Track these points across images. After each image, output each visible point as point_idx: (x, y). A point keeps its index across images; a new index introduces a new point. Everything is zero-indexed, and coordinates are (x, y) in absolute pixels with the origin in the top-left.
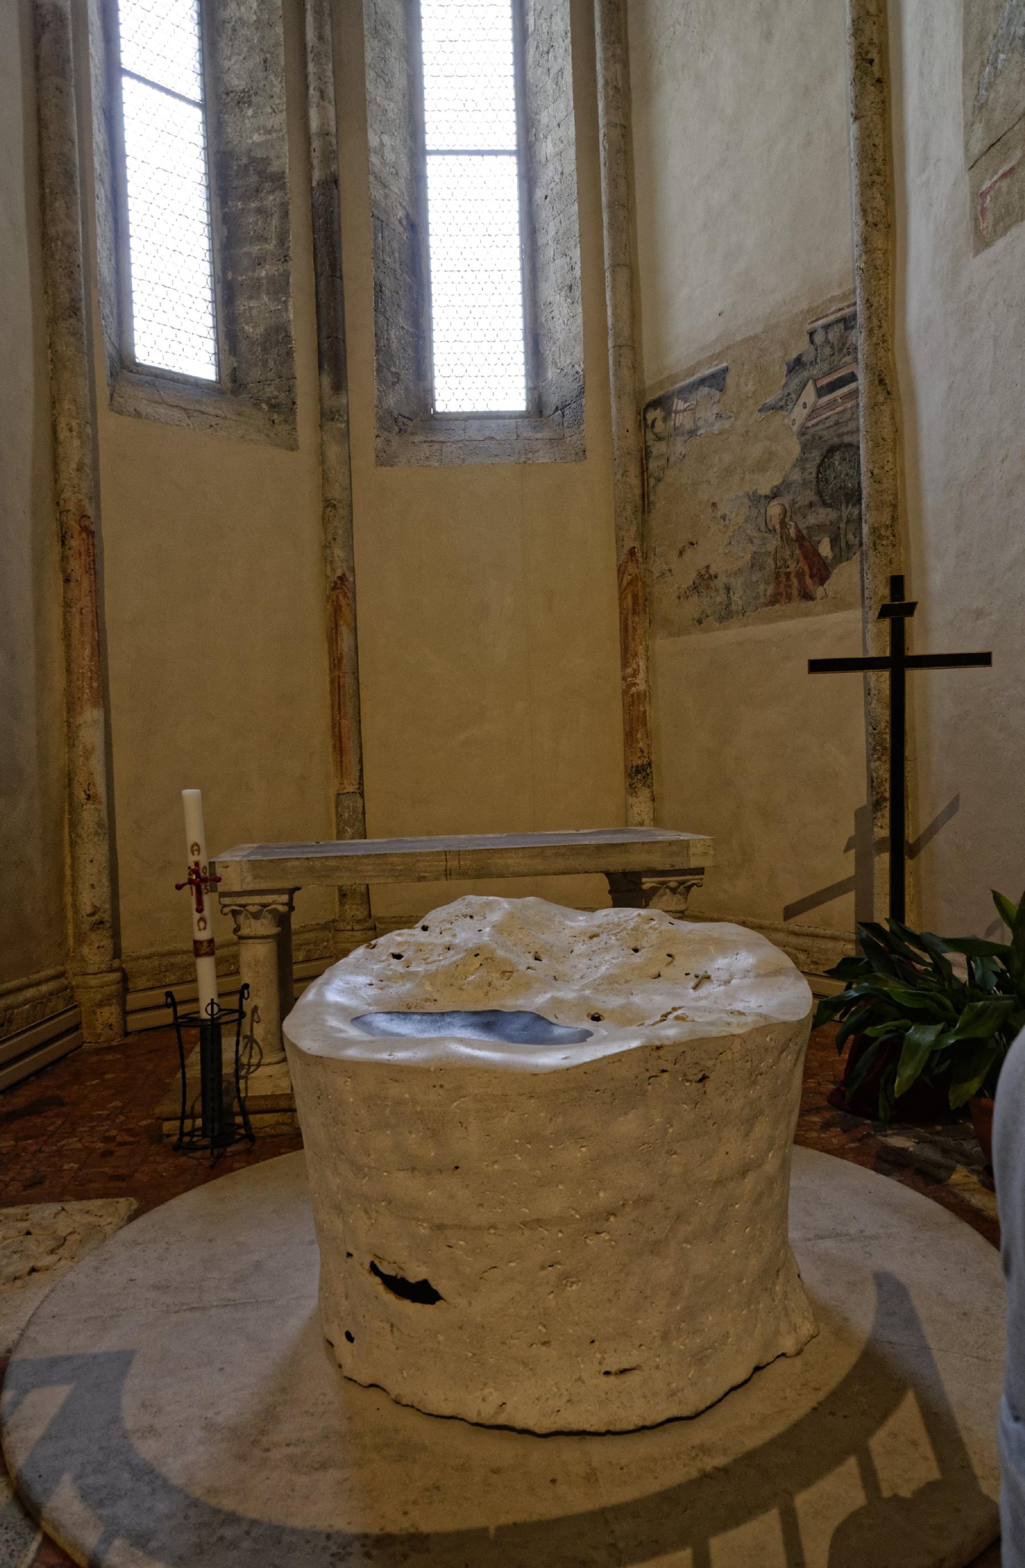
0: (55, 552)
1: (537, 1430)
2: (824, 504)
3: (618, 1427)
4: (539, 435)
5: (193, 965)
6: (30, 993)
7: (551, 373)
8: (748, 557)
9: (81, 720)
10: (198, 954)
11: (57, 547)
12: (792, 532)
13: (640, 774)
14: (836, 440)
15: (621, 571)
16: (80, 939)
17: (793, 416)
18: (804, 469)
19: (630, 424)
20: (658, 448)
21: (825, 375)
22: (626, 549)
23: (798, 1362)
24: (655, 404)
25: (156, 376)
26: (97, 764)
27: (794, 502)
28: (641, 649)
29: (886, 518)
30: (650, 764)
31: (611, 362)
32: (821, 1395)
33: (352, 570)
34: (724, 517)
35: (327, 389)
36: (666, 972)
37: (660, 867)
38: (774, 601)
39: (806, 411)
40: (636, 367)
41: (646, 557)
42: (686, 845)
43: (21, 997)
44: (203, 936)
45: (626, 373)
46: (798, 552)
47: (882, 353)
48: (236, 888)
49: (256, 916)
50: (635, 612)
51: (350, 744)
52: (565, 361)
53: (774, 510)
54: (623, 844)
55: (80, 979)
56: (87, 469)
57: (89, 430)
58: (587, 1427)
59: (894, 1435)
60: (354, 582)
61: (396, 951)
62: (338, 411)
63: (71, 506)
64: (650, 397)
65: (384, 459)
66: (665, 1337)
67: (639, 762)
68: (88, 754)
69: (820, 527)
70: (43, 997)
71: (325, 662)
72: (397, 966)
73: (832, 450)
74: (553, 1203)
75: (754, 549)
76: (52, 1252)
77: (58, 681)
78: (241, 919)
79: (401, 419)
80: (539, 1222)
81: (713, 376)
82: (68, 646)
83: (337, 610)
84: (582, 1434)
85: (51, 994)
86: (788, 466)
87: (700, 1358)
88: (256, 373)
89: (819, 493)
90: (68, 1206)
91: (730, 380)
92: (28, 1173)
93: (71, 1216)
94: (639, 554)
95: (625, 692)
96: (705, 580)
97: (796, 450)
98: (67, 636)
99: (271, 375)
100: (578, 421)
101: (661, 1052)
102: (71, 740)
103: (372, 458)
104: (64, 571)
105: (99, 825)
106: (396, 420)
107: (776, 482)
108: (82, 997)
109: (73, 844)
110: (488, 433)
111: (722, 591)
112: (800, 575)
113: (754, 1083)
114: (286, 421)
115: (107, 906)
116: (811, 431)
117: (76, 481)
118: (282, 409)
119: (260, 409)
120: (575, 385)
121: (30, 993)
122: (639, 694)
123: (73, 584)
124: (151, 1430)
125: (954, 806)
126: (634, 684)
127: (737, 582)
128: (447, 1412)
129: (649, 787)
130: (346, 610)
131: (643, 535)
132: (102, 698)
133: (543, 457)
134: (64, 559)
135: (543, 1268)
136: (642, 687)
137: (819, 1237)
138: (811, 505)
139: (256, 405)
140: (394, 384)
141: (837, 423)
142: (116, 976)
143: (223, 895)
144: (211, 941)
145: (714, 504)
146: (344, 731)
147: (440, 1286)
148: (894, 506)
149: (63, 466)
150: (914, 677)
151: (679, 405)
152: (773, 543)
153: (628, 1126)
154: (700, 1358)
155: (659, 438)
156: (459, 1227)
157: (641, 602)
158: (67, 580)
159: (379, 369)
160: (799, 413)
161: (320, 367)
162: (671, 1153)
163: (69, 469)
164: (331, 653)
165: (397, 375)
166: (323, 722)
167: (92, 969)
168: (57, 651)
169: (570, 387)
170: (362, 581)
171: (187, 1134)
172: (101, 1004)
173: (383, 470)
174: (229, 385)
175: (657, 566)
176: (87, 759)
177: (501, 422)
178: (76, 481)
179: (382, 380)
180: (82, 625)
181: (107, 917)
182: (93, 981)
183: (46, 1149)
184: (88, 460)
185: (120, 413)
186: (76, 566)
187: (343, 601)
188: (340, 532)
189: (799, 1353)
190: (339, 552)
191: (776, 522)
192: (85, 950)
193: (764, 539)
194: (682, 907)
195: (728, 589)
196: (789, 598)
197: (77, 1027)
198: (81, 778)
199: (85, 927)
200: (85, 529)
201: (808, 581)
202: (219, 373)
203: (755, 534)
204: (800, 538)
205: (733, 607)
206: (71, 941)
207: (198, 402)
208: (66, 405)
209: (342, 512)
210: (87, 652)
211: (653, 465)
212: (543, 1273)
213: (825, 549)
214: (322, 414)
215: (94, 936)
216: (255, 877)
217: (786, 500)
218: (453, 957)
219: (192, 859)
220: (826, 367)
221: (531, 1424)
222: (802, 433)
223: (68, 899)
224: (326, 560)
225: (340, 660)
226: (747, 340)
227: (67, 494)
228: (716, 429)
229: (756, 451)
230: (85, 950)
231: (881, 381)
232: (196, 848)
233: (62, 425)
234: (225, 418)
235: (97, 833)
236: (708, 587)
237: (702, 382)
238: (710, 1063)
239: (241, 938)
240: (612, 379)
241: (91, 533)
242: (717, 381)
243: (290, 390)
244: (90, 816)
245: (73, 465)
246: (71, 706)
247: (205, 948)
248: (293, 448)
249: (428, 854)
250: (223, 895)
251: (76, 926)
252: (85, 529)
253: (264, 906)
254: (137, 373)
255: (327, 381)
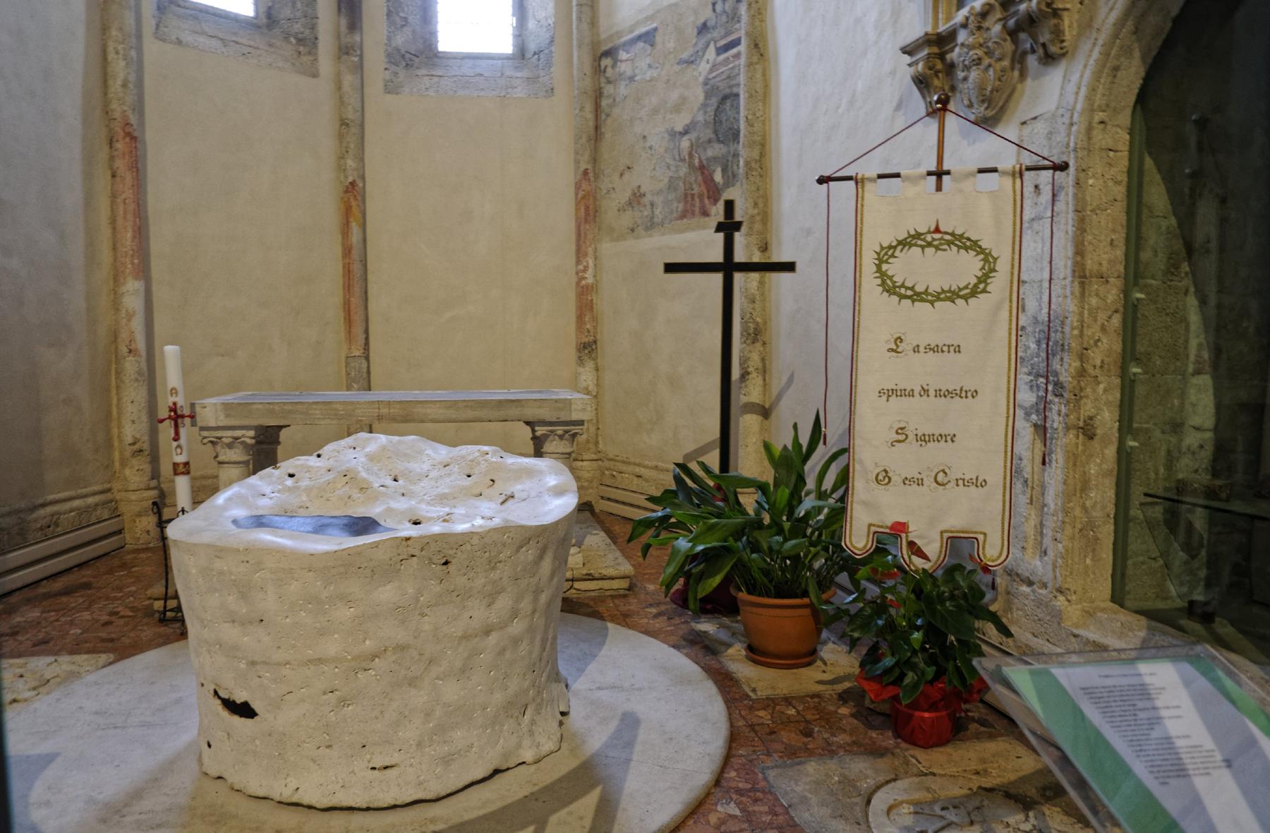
0: (103, 154)
1: (318, 806)
2: (719, 141)
3: (376, 805)
4: (519, 75)
5: (173, 481)
6: (76, 503)
7: (531, 24)
8: (666, 180)
9: (124, 289)
10: (176, 474)
11: (106, 149)
12: (696, 162)
13: (588, 348)
14: (728, 91)
15: (578, 186)
16: (124, 463)
17: (700, 69)
18: (706, 112)
19: (588, 69)
20: (608, 90)
21: (722, 38)
22: (582, 169)
23: (533, 767)
24: (607, 54)
25: (201, 11)
26: (137, 325)
27: (698, 138)
28: (590, 250)
29: (755, 154)
30: (595, 342)
31: (574, 17)
32: (536, 788)
33: (363, 178)
34: (651, 148)
35: (344, 28)
36: (486, 492)
37: (548, 419)
38: (683, 216)
39: (708, 66)
40: (593, 23)
41: (597, 177)
42: (568, 403)
43: (68, 506)
44: (180, 459)
45: (585, 26)
46: (700, 178)
47: (757, 23)
48: (212, 424)
49: (230, 446)
50: (586, 221)
51: (358, 318)
52: (541, 14)
53: (685, 143)
54: (519, 401)
55: (123, 494)
56: (131, 86)
57: (133, 53)
58: (354, 805)
59: (570, 813)
60: (364, 187)
61: (291, 472)
62: (352, 47)
63: (117, 115)
64: (604, 48)
65: (391, 88)
66: (419, 745)
67: (586, 340)
68: (130, 317)
69: (715, 159)
70: (89, 507)
71: (339, 250)
72: (290, 482)
73: (725, 98)
74: (332, 647)
75: (671, 174)
76: (34, 689)
77: (106, 256)
78: (218, 448)
79: (408, 56)
80: (320, 661)
81: (647, 34)
82: (114, 229)
83: (347, 211)
84: (351, 809)
85: (97, 505)
86: (695, 109)
87: (446, 761)
88: (287, 12)
89: (716, 132)
90: (60, 659)
91: (659, 39)
92: (41, 636)
93: (65, 663)
94: (591, 175)
95: (578, 284)
96: (637, 197)
97: (701, 97)
98: (113, 221)
99: (298, 14)
100: (549, 64)
101: (409, 542)
102: (116, 305)
103: (380, 85)
104: (111, 169)
105: (139, 373)
106: (403, 56)
107: (687, 122)
108: (123, 508)
109: (118, 387)
110: (478, 71)
111: (649, 207)
112: (701, 196)
113: (494, 568)
114: (310, 53)
115: (146, 438)
116: (711, 82)
117: (121, 95)
118: (307, 43)
119: (290, 42)
120: (548, 35)
121: (76, 503)
122: (587, 286)
123: (118, 179)
124: (48, 804)
125: (790, 380)
126: (584, 278)
127: (659, 200)
128: (261, 794)
129: (595, 359)
130: (355, 210)
131: (594, 160)
132: (144, 271)
133: (520, 93)
134: (112, 158)
135: (325, 693)
136: (590, 280)
137: (599, 688)
138: (710, 141)
139: (286, 39)
140: (403, 26)
141: (729, 77)
142: (154, 493)
143: (202, 429)
144: (186, 464)
145: (645, 137)
146: (352, 307)
147: (255, 706)
148: (763, 145)
149: (110, 82)
150: (717, 279)
151: (623, 55)
152: (684, 170)
153: (386, 594)
154: (446, 761)
155: (609, 82)
156: (265, 663)
157: (592, 213)
158: (114, 176)
159: (389, 14)
160: (704, 67)
161: (339, 9)
162: (423, 615)
163: (116, 86)
164: (343, 245)
165: (405, 19)
166: (338, 299)
167: (132, 487)
168: (106, 232)
169: (545, 36)
170: (372, 189)
171: (171, 610)
172: (139, 515)
173: (389, 97)
174: (265, 21)
175: (605, 185)
176: (129, 320)
177: (491, 62)
178: (121, 95)
179: (391, 22)
180: (125, 212)
181: (146, 446)
182: (133, 496)
183: (63, 619)
184: (132, 78)
185: (164, 40)
186: (120, 164)
187: (354, 203)
188: (352, 146)
189: (537, 762)
190: (350, 163)
191: (685, 154)
192: (127, 472)
193: (677, 166)
194: (568, 450)
195: (652, 205)
196: (693, 214)
197: (120, 532)
198: (124, 335)
199: (128, 454)
200: (128, 134)
201: (706, 201)
202: (257, 11)
203: (671, 162)
204: (702, 167)
205: (656, 220)
206: (117, 464)
207: (235, 34)
208: (114, 33)
209: (353, 130)
210: (129, 235)
211: (604, 103)
212: (325, 697)
213: (718, 177)
214: (340, 49)
215: (135, 461)
216: (227, 416)
217: (693, 136)
218: (331, 476)
219: (171, 400)
220: (723, 32)
221: (314, 802)
222: (706, 84)
223: (115, 431)
224: (341, 168)
225: (350, 251)
226: (670, 6)
227: (114, 105)
228: (648, 77)
229: (674, 96)
230: (127, 472)
231: (756, 46)
232: (174, 391)
233: (111, 49)
234: (257, 48)
235: (137, 380)
236: (639, 203)
237: (639, 38)
238: (451, 552)
239: (220, 463)
240: (575, 31)
241: (134, 138)
242: (648, 38)
243: (313, 27)
244: (131, 366)
245: (119, 82)
246: (117, 278)
247: (181, 469)
248: (315, 75)
249: (365, 403)
250: (202, 429)
251: (121, 453)
252: (128, 134)
253: (237, 438)
254: (185, 7)
255: (344, 22)
